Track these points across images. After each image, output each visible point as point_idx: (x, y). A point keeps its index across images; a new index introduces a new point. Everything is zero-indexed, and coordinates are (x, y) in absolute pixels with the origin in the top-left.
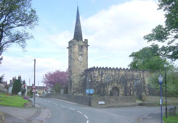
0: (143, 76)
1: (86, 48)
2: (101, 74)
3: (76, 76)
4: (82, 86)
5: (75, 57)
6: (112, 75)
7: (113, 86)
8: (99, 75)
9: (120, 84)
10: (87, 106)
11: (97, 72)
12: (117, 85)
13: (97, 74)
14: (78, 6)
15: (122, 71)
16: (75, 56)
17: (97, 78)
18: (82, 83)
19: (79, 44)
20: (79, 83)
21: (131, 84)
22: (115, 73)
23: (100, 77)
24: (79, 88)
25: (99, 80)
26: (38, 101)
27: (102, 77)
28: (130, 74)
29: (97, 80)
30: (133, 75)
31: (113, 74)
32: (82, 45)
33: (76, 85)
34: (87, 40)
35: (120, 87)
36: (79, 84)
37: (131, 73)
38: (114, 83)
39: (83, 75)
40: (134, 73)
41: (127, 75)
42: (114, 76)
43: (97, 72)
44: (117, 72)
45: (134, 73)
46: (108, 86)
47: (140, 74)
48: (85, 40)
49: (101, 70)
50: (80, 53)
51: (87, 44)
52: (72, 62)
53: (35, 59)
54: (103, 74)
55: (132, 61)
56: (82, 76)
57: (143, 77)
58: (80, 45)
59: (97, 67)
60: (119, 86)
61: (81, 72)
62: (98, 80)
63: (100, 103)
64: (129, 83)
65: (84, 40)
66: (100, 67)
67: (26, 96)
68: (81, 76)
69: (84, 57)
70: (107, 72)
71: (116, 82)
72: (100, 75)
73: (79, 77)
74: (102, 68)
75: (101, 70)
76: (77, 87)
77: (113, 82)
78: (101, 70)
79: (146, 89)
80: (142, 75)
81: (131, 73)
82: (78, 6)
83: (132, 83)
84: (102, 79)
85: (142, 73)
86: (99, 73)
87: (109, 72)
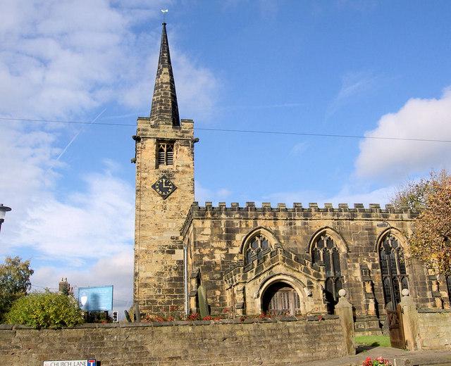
2: (227, 231)
3: (146, 252)
4: (170, 291)
5: (144, 182)
7: (266, 275)
8: (215, 239)
11: (208, 223)
12: (290, 272)
13: (208, 231)
16: (145, 179)
17: (206, 251)
19: (160, 135)
20: (159, 279)
21: (363, 268)
22: (291, 224)
23: (223, 244)
24: (160, 300)
25: (219, 256)
26: (113, 335)
27: (229, 244)
28: (357, 227)
29: (206, 259)
30: (371, 230)
32: (173, 141)
33: (146, 285)
35: (305, 280)
37: (363, 223)
39: (174, 248)
41: (343, 231)
42: (287, 239)
43: (208, 223)
44: (299, 223)
46: (245, 277)
49: (227, 214)
53: (9, 209)
54: (235, 231)
56: (173, 252)
58: (162, 140)
62: (211, 255)
64: (357, 265)
68: (169, 252)
70: (251, 222)
71: (280, 256)
72: (220, 236)
73: (160, 253)
75: (223, 216)
76: (152, 293)
77: (268, 260)
78: (223, 216)
79: (435, 288)
81: (363, 223)
83: (370, 266)
84: (231, 251)
86: (215, 226)
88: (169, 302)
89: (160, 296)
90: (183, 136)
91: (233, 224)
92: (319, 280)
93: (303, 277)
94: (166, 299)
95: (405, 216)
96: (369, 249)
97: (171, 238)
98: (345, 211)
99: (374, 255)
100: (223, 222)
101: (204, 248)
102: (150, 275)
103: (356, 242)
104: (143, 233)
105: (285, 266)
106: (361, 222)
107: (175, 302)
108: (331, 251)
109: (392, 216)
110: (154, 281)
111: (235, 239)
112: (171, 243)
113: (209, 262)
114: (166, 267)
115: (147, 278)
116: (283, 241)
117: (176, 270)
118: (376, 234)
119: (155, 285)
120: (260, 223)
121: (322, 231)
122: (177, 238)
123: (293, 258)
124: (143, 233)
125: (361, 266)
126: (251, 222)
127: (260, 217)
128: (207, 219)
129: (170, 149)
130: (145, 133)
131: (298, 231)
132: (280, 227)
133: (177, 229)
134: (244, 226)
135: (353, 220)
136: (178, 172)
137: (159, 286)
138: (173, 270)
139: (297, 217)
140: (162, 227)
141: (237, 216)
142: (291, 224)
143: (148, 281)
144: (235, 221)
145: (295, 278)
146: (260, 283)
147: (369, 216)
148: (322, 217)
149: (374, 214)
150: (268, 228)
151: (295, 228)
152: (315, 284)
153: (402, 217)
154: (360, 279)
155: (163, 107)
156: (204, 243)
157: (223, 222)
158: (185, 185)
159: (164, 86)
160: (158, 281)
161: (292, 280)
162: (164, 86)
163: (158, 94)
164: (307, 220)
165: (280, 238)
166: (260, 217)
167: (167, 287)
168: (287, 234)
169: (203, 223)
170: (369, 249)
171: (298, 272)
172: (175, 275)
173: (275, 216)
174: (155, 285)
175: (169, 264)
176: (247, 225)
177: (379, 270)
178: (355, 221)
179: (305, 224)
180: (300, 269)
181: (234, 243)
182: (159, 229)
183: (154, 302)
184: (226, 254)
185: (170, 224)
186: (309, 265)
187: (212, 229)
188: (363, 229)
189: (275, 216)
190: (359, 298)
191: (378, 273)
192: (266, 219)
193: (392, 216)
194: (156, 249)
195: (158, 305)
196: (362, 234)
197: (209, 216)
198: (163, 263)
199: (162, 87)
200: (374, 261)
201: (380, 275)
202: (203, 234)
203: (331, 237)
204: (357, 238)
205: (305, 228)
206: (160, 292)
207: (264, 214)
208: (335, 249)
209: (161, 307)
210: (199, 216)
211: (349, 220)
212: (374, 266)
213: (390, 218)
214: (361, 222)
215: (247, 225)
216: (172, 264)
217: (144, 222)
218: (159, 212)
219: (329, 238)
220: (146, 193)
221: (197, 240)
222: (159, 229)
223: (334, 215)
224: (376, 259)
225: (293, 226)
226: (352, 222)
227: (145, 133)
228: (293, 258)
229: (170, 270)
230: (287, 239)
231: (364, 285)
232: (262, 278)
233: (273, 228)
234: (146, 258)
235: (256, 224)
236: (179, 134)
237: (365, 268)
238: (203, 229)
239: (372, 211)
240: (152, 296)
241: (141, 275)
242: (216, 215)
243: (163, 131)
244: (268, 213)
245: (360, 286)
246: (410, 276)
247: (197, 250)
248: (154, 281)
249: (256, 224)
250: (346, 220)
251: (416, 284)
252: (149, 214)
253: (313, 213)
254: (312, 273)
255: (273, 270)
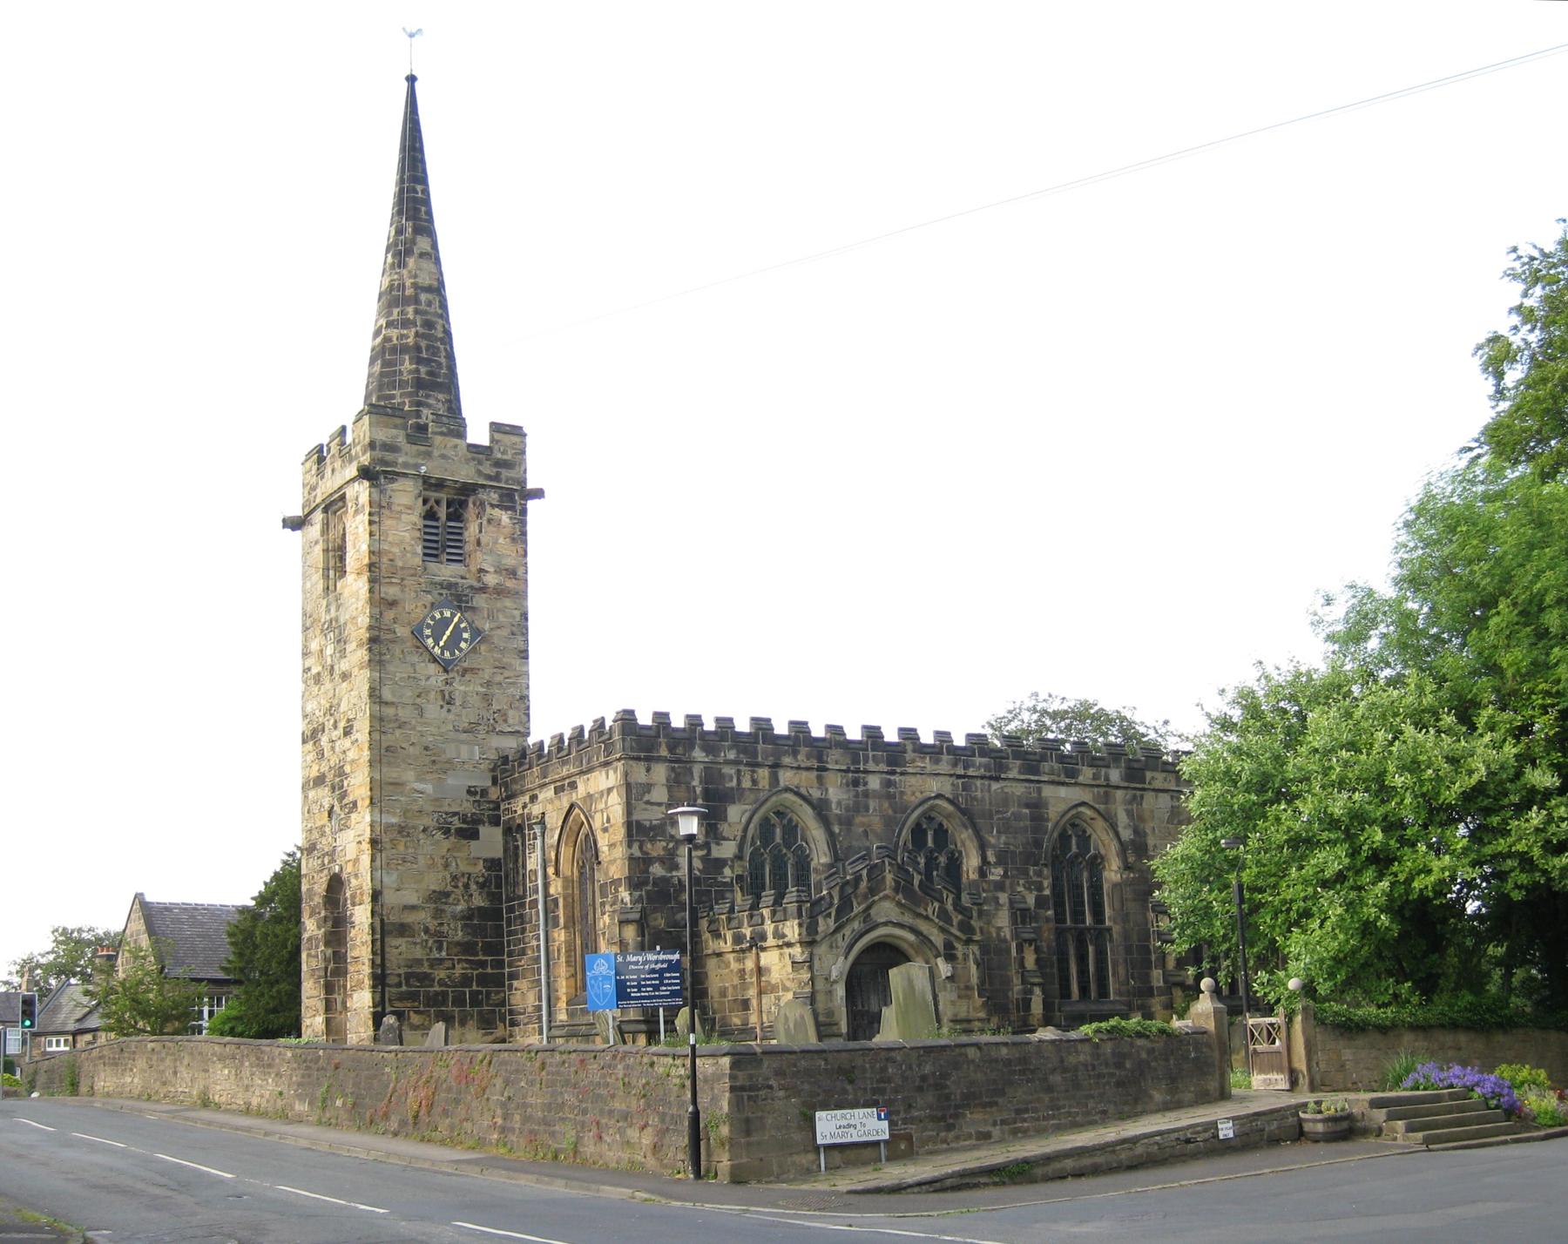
0: (1137, 820)
1: (505, 517)
4: (467, 948)
6: (821, 809)
7: (856, 925)
9: (932, 908)
10: (840, 1172)
12: (908, 919)
14: (412, 79)
15: (927, 764)
16: (393, 604)
18: (468, 916)
20: (438, 913)
22: (856, 783)
24: (441, 974)
28: (1006, 800)
29: (657, 870)
30: (1037, 807)
31: (836, 793)
32: (468, 489)
34: (517, 431)
36: (432, 925)
37: (1018, 790)
38: (872, 891)
40: (1048, 791)
42: (847, 822)
44: (874, 783)
45: (1048, 791)
47: (1107, 799)
48: (496, 428)
50: (446, 571)
51: (512, 474)
52: (345, 676)
55: (1443, 487)
57: (1136, 831)
58: (440, 485)
59: (662, 718)
60: (924, 927)
61: (457, 782)
62: (670, 861)
63: (830, 1126)
64: (1003, 898)
65: (478, 434)
66: (694, 721)
67: (407, 357)
68: (461, 833)
69: (491, 616)
70: (763, 774)
73: (439, 836)
74: (709, 725)
76: (419, 953)
78: (698, 754)
80: (1122, 818)
81: (1018, 790)
82: (412, 79)
83: (1031, 900)
85: (1119, 794)
87: (786, 777)
88: (466, 980)
89: (441, 961)
90: (497, 478)
91: (722, 776)
92: (968, 942)
93: (935, 931)
94: (458, 971)
95: (1115, 775)
96: (1030, 858)
97: (469, 792)
98: (981, 755)
99: (1039, 874)
100: (697, 770)
101: (653, 840)
102: (413, 899)
103: (1003, 838)
104: (392, 774)
105: (899, 904)
106: (1015, 787)
107: (483, 980)
108: (943, 860)
109: (1086, 774)
110: (423, 917)
111: (725, 819)
112: (467, 807)
113: (665, 880)
114: (454, 878)
115: (406, 907)
116: (836, 829)
117: (482, 886)
118: (1048, 820)
119: (427, 930)
120: (786, 777)
121: (926, 806)
122: (484, 792)
123: (916, 882)
124: (392, 774)
125: (1011, 902)
126: (763, 774)
127: (787, 760)
128: (659, 759)
129: (456, 515)
130: (389, 456)
131: (872, 804)
132: (831, 790)
133: (485, 766)
134: (746, 784)
135: (997, 779)
136: (483, 589)
137: (439, 934)
138: (473, 887)
139: (871, 766)
140: (443, 758)
141: (732, 755)
142: (856, 783)
143: (409, 918)
144: (729, 770)
145: (913, 930)
146: (844, 944)
147: (1036, 771)
148: (928, 770)
149: (1046, 766)
150: (803, 791)
151: (866, 794)
152: (960, 949)
153: (1107, 779)
154: (1007, 933)
155: (423, 370)
156: (652, 828)
157: (697, 770)
158: (505, 632)
159: (423, 297)
160: (434, 918)
161: (911, 937)
162: (423, 297)
163: (406, 323)
164: (893, 773)
165: (832, 819)
166: (787, 760)
167: (460, 936)
168: (848, 809)
169: (648, 770)
170: (1030, 858)
171: (927, 918)
172: (479, 901)
173: (820, 759)
174: (427, 930)
175: (464, 868)
176: (754, 782)
177: (1050, 913)
178: (1002, 784)
179: (889, 784)
180: (930, 910)
181: (724, 828)
182: (436, 763)
183: (425, 978)
184: (704, 859)
185: (464, 749)
186: (950, 901)
187: (670, 788)
188: (1019, 805)
189: (820, 759)
190: (1007, 982)
191: (1048, 920)
192: (799, 768)
193: (1086, 774)
194: (428, 821)
195: (437, 988)
196: (1017, 817)
197: (664, 752)
198: (446, 866)
199: (417, 301)
200: (1040, 888)
201: (1052, 925)
202: (648, 802)
203: (945, 823)
204: (1005, 828)
205: (890, 797)
206: (440, 949)
207: (795, 753)
208: (952, 853)
209: (445, 994)
210: (641, 750)
211: (991, 778)
212: (1041, 902)
213: (1081, 779)
214: (1015, 787)
215: (754, 782)
216: (470, 869)
217: (395, 737)
218: (433, 710)
219: (941, 825)
220: (397, 650)
221: (635, 817)
222: (436, 763)
223: (955, 765)
224: (1046, 883)
225: (861, 788)
226: (995, 786)
227: (389, 456)
228: (916, 882)
229: (467, 886)
230: (847, 822)
231: (1020, 949)
232: (847, 931)
233: (816, 794)
234: (401, 848)
235: (774, 779)
236: (488, 469)
237: (1022, 906)
238: (648, 787)
239: (1043, 758)
240: (419, 962)
241: (390, 898)
242: (680, 750)
243: (443, 456)
244: (804, 750)
245: (1008, 951)
246: (1116, 929)
247: (636, 846)
248: (423, 917)
249: (774, 779)
250: (982, 777)
251: (1128, 950)
252: (405, 714)
253: (909, 755)
254: (955, 923)
255: (873, 912)
